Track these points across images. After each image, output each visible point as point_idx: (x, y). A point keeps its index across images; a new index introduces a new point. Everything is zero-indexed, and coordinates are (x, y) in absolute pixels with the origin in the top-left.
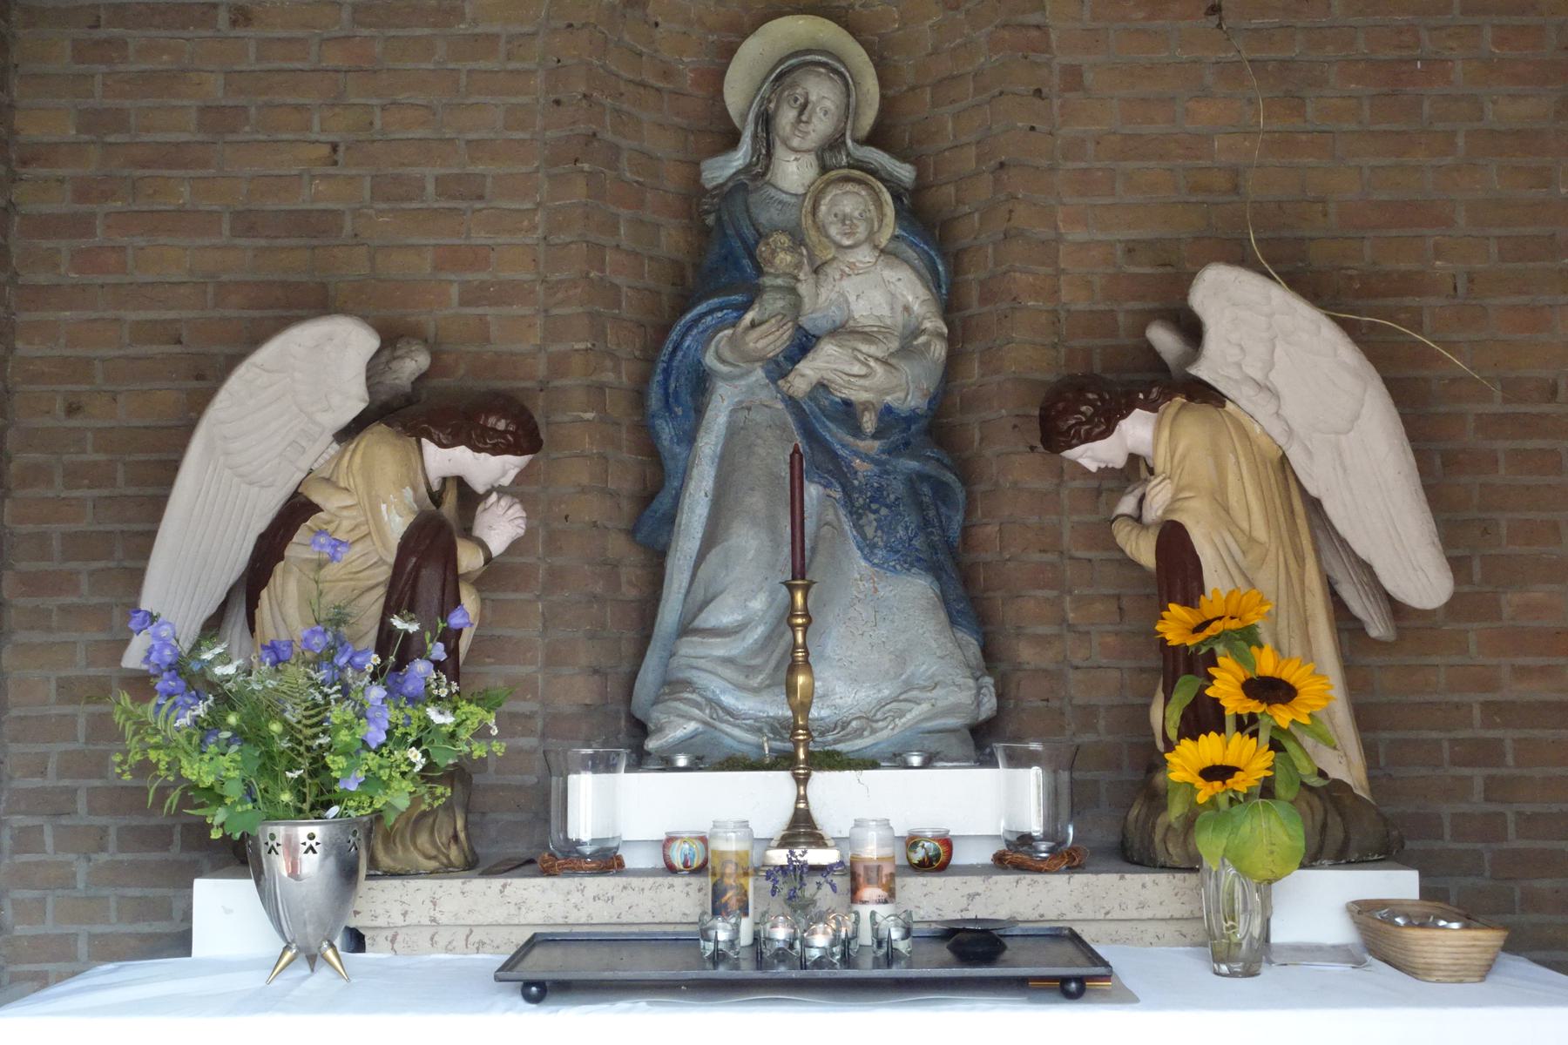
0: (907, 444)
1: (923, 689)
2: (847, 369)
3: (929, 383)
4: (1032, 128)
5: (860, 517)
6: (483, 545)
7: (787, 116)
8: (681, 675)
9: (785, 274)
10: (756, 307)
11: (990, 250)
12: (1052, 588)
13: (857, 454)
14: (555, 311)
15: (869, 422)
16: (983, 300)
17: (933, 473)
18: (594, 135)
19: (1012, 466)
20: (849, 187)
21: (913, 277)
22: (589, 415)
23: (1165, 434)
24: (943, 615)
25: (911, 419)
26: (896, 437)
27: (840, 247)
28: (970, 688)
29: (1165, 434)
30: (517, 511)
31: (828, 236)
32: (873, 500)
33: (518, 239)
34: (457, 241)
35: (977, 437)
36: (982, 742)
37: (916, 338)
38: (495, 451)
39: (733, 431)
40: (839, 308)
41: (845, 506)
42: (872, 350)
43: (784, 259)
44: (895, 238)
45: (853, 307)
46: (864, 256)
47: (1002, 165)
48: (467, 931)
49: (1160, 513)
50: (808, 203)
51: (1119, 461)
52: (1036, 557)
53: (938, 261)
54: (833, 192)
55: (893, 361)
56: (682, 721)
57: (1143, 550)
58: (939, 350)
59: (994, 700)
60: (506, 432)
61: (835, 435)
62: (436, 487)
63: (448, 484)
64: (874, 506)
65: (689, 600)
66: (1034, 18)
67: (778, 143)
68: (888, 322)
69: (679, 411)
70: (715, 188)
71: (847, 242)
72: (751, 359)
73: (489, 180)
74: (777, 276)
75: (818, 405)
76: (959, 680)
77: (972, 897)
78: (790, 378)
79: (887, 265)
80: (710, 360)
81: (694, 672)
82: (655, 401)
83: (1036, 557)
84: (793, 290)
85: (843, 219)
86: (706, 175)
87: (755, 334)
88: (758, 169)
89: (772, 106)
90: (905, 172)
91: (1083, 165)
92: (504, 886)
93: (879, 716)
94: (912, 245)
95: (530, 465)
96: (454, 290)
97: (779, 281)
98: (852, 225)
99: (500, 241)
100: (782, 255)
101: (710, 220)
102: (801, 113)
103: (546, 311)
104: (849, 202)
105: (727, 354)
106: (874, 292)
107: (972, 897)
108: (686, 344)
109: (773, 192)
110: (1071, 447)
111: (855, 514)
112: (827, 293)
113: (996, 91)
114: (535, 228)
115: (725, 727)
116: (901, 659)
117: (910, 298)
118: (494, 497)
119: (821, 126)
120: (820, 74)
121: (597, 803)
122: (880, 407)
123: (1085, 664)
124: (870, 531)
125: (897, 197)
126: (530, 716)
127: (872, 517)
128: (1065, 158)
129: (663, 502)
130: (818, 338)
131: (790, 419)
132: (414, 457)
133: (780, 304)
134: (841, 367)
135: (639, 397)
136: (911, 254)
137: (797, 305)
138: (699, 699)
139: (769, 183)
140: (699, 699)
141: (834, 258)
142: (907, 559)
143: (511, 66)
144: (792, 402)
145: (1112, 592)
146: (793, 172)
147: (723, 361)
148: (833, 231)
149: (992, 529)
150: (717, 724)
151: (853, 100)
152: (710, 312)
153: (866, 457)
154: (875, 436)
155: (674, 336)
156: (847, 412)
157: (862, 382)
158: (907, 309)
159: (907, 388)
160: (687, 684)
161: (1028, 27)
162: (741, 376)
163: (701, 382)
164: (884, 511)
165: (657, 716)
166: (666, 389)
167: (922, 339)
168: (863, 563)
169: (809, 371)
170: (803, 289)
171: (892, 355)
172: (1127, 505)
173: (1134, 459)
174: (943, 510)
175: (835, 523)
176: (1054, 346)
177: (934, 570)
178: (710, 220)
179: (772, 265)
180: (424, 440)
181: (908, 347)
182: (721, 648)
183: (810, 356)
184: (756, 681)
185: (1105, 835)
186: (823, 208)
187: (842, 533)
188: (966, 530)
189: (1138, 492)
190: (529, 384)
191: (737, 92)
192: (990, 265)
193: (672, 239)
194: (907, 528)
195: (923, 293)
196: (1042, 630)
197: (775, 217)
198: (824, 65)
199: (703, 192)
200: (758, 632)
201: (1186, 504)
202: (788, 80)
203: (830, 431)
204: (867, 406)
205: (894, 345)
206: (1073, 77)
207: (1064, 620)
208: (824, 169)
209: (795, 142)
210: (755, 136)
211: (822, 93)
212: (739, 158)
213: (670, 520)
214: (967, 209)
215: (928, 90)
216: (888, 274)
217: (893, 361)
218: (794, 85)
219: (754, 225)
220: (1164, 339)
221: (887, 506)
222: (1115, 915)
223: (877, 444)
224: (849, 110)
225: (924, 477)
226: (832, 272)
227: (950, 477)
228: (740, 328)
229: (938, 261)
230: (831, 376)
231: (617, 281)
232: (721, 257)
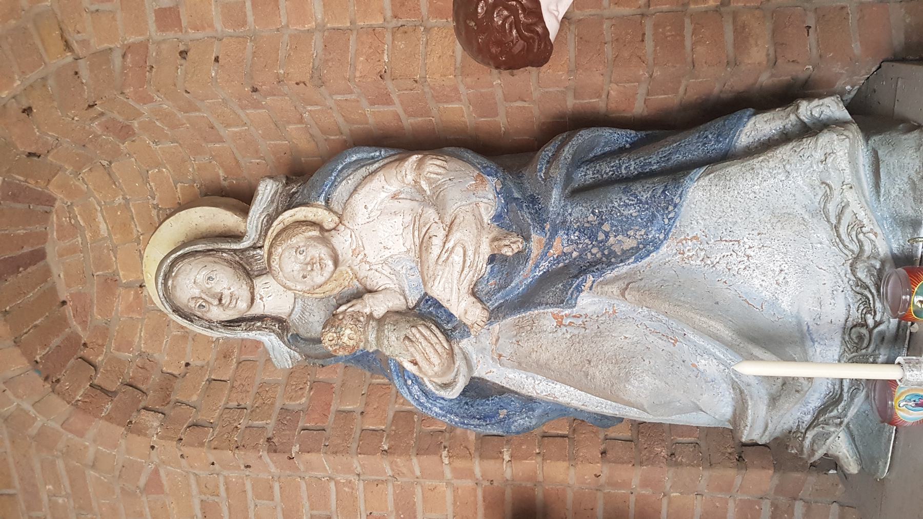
1: (827, 198)
2: (458, 268)
4: (217, 60)
5: (612, 253)
12: (682, 27)
13: (544, 255)
15: (511, 247)
16: (388, 101)
17: (564, 171)
25: (505, 193)
26: (526, 216)
32: (593, 236)
33: (360, 494)
35: (519, 104)
41: (602, 272)
42: (437, 242)
44: (328, 206)
52: (649, 44)
53: (348, 160)
55: (448, 220)
59: (827, 101)
64: (601, 236)
68: (408, 218)
73: (315, 512)
76: (819, 155)
80: (454, 393)
83: (649, 44)
84: (381, 321)
94: (334, 185)
99: (362, 508)
111: (609, 260)
116: (782, 217)
117: (383, 195)
120: (174, 287)
122: (496, 232)
124: (629, 243)
126: (775, 506)
127: (612, 240)
128: (244, 23)
131: (510, 320)
134: (456, 275)
153: (549, 245)
154: (527, 239)
157: (470, 253)
158: (394, 197)
164: (606, 227)
168: (663, 249)
176: (427, 30)
181: (436, 201)
190: (480, 493)
192: (353, 97)
194: (626, 205)
195: (378, 182)
196: (729, 36)
197: (317, 318)
207: (716, 10)
216: (361, 216)
223: (535, 237)
225: (568, 178)
229: (348, 160)
231: (391, 414)
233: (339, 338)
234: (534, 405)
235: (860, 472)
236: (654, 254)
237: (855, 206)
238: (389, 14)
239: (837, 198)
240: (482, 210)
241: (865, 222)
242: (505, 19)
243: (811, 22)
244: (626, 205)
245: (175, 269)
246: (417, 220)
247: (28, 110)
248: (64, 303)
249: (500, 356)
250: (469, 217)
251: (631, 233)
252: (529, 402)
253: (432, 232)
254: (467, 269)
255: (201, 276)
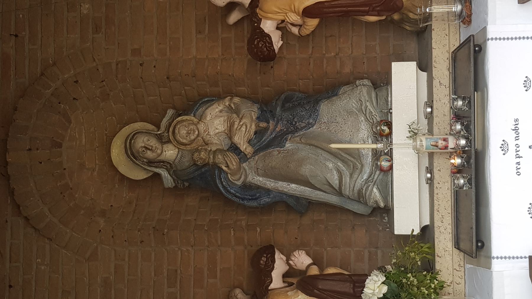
0: (271, 112)
1: (361, 105)
2: (244, 132)
3: (249, 104)
4: (155, 67)
5: (297, 128)
6: (309, 266)
7: (150, 155)
8: (356, 195)
9: (209, 155)
10: (220, 165)
11: (199, 83)
14: (219, 243)
15: (263, 125)
17: (282, 102)
18: (154, 228)
19: (280, 73)
20: (177, 131)
21: (210, 109)
22: (258, 229)
23: (270, 15)
24: (334, 98)
27: (198, 135)
28: (362, 88)
29: (270, 15)
30: (296, 253)
31: (194, 140)
34: (192, 280)
35: (267, 88)
36: (382, 82)
37: (232, 108)
38: (274, 261)
39: (266, 175)
40: (221, 136)
41: (294, 134)
43: (203, 155)
44: (194, 116)
45: (220, 131)
46: (202, 127)
47: (168, 78)
48: (455, 271)
49: (299, 18)
50: (182, 147)
51: (279, 33)
54: (178, 137)
55: (241, 116)
56: (373, 194)
57: (313, 23)
58: (236, 100)
59: (365, 80)
60: (266, 257)
61: (267, 137)
62: (286, 285)
63: (285, 280)
64: (294, 123)
65: (328, 191)
66: (114, 66)
67: (159, 158)
68: (226, 118)
69: (258, 195)
70: (175, 182)
71: (197, 133)
72: (239, 168)
73: (170, 268)
74: (210, 157)
75: (257, 143)
76: (358, 92)
77: (441, 84)
78: (247, 153)
79: (205, 118)
80: (239, 183)
81: (355, 189)
82: (254, 204)
83: (312, 66)
84: (215, 152)
85: (188, 133)
86: (170, 185)
87: (231, 166)
88: (168, 166)
89: (145, 160)
90: (170, 112)
91: (168, 48)
92: (438, 256)
93: (371, 121)
94: (197, 110)
95: (277, 249)
96: (211, 281)
97: (211, 157)
98: (191, 130)
100: (202, 156)
101: (186, 184)
102: (149, 149)
103: (219, 246)
104: (182, 132)
105: (237, 177)
106: (214, 122)
107: (441, 84)
108: (234, 192)
109: (177, 161)
110: (274, 50)
111: (297, 130)
112: (215, 141)
113: (141, 80)
114: (188, 250)
115: (375, 178)
116: (350, 113)
117: (217, 110)
118: (291, 262)
119: (153, 142)
121: (407, 220)
123: (351, 49)
125: (180, 115)
126: (370, 252)
127: (297, 124)
129: (291, 202)
130: (232, 143)
132: (276, 292)
133: (220, 156)
134: (243, 135)
135: (251, 211)
136: (200, 110)
137: (220, 151)
138: (365, 187)
139: (173, 162)
140: (365, 187)
141: (202, 138)
142: (314, 111)
143: (127, 259)
144: (256, 153)
145: (324, 40)
146: (170, 153)
147: (240, 178)
148: (193, 138)
149: (301, 82)
150: (374, 180)
151: (144, 131)
152: (222, 183)
154: (268, 123)
155: (230, 197)
156: (259, 133)
157: (248, 127)
158: (221, 111)
159: (251, 112)
160: (360, 192)
161: (117, 68)
162: (246, 172)
163: (247, 187)
164: (296, 120)
165: (371, 203)
166: (250, 199)
167: (232, 106)
168: (315, 127)
169: (244, 147)
170: (214, 149)
171: (238, 117)
172: (295, 30)
173: (278, 28)
174: (294, 99)
175: (300, 137)
176: (234, 60)
177: (317, 102)
178: (186, 184)
179: (205, 160)
180: (269, 288)
181: (236, 111)
182: (346, 179)
183: (239, 146)
184: (359, 166)
185: (412, 46)
186: (184, 141)
187: (303, 134)
188: (300, 92)
189: (290, 26)
190: (246, 252)
191: (138, 175)
193: (191, 201)
198: (131, 140)
199: (176, 187)
200: (340, 164)
201: (296, 7)
202: (136, 154)
203: (266, 139)
204: (257, 126)
205: (235, 115)
206: (136, 52)
208: (169, 141)
209: (159, 152)
210: (156, 167)
211: (141, 142)
212: (164, 173)
213: (297, 199)
214: (183, 92)
215: (138, 106)
217: (241, 116)
218: (138, 152)
219: (189, 167)
220: (234, 17)
221: (294, 118)
222: (447, 32)
223: (271, 122)
224: (148, 133)
225: (283, 106)
226: (207, 138)
227: (283, 97)
228: (229, 171)
230: (246, 138)
231: (208, 220)
232: (201, 179)
233: (200, 155)
234: (270, 193)
235: (405, 239)
236: (311, 128)
237: (369, 107)
238: (220, 54)
239: (364, 105)
240: (253, 115)
241: (373, 112)
242: (263, 45)
243: (365, 61)
244: (302, 111)
245: (135, 136)
246: (229, 119)
247: (76, 82)
248: (65, 169)
249: (258, 169)
250: (248, 115)
251: (304, 121)
252: (268, 191)
253: (235, 120)
254: (247, 133)
255: (146, 139)
